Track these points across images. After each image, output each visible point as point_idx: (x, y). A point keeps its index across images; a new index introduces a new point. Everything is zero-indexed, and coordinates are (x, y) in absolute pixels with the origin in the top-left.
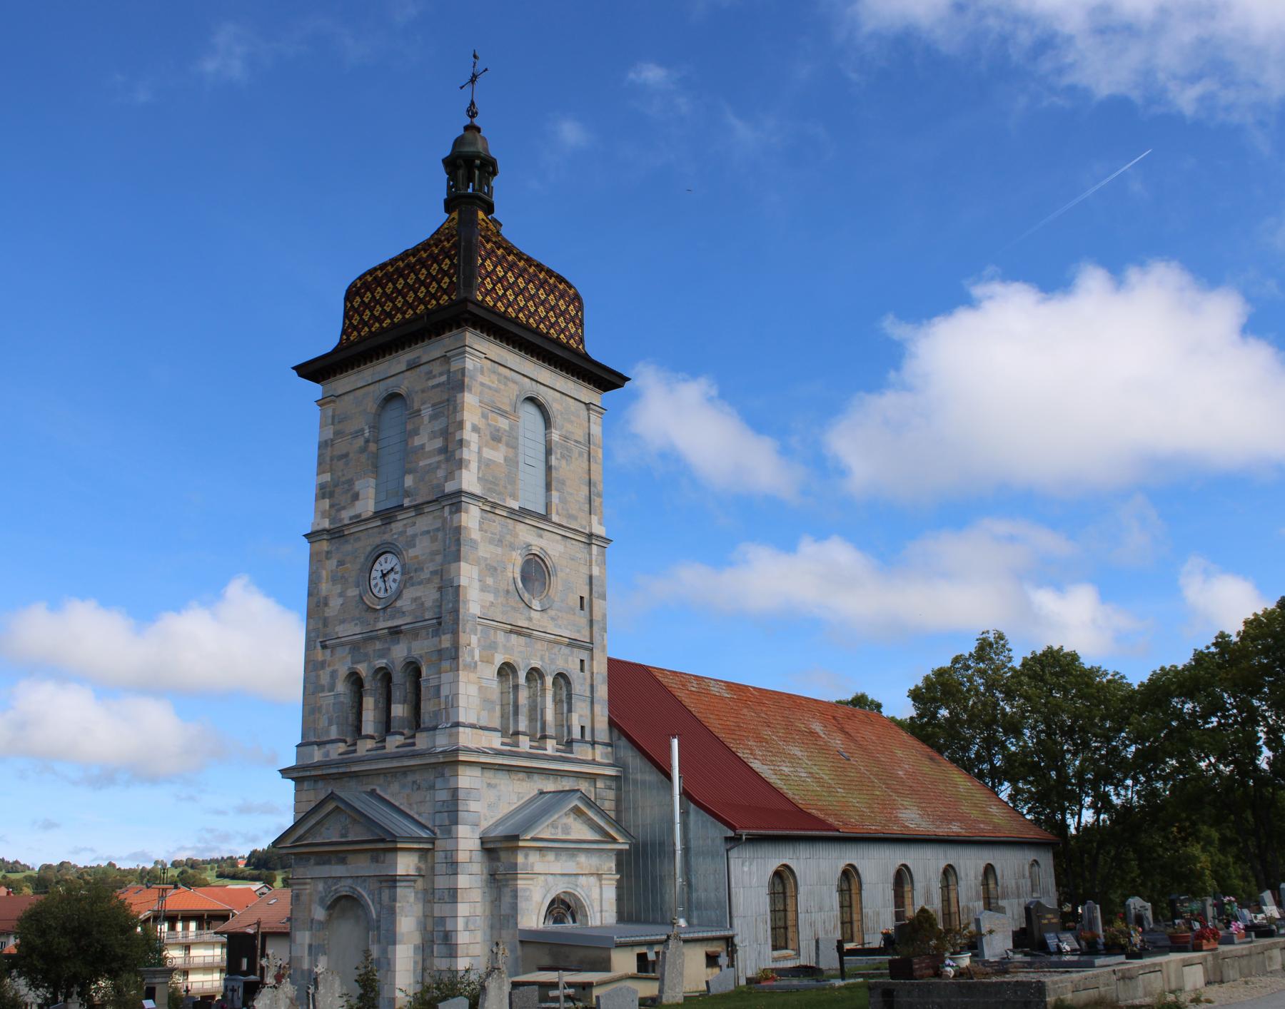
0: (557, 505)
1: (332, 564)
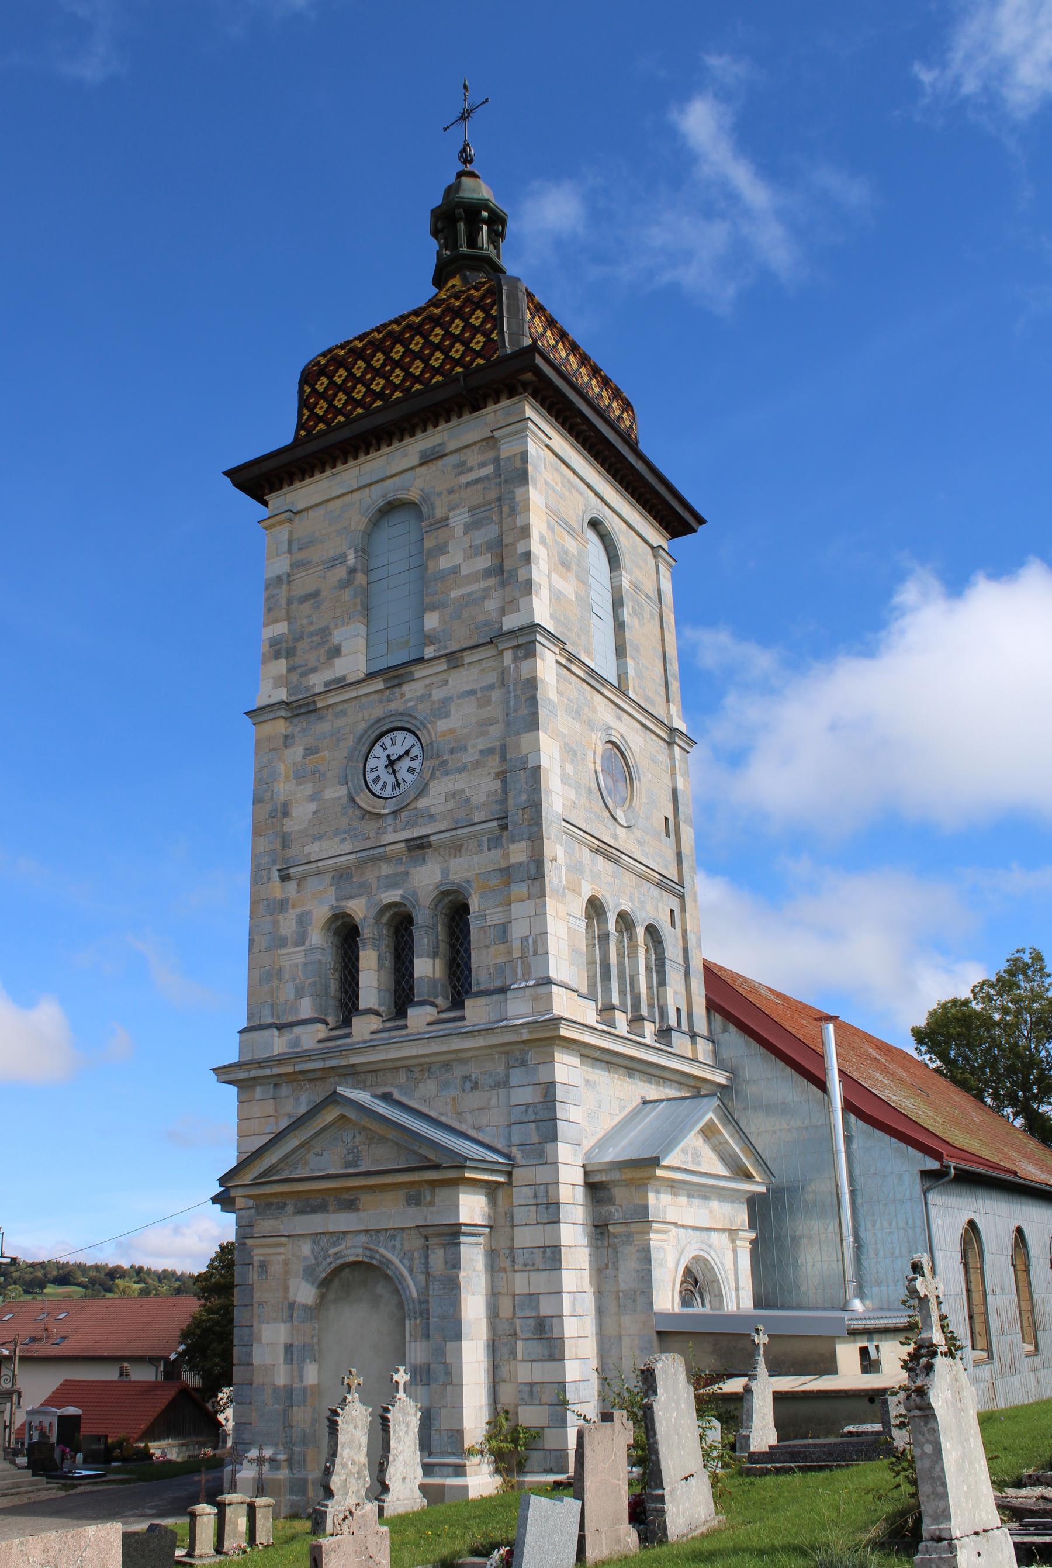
0: (633, 678)
1: (296, 752)
